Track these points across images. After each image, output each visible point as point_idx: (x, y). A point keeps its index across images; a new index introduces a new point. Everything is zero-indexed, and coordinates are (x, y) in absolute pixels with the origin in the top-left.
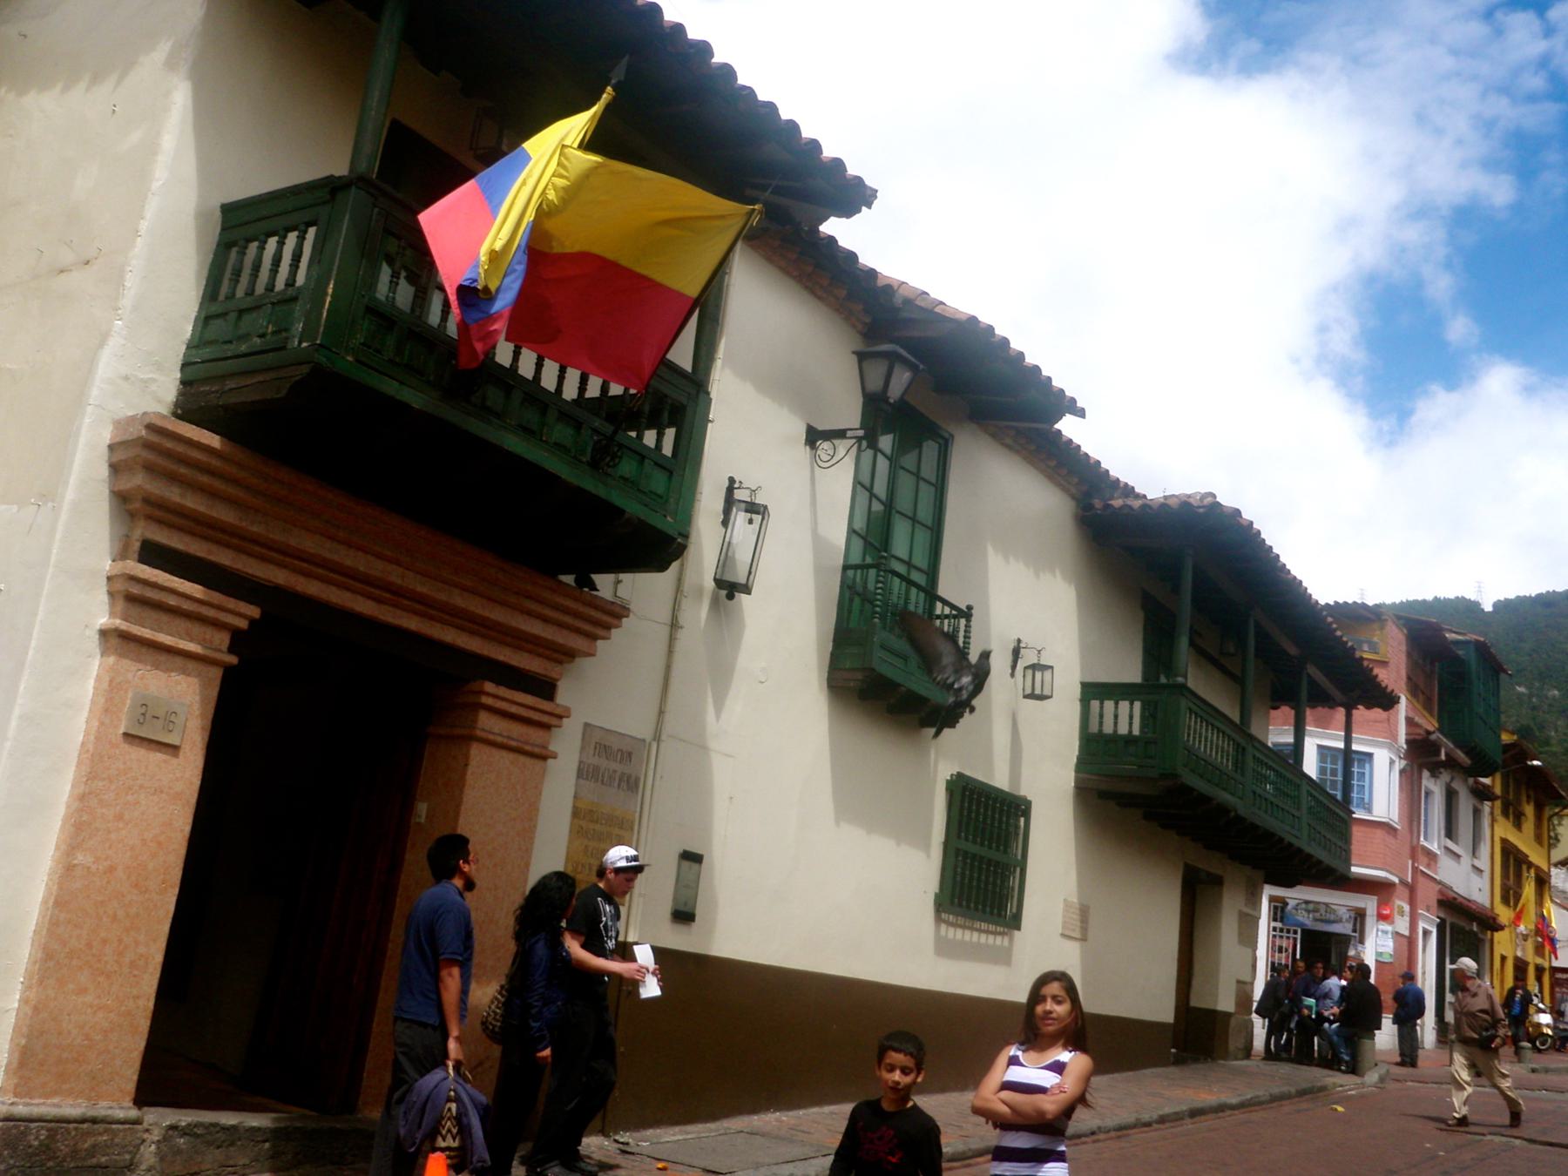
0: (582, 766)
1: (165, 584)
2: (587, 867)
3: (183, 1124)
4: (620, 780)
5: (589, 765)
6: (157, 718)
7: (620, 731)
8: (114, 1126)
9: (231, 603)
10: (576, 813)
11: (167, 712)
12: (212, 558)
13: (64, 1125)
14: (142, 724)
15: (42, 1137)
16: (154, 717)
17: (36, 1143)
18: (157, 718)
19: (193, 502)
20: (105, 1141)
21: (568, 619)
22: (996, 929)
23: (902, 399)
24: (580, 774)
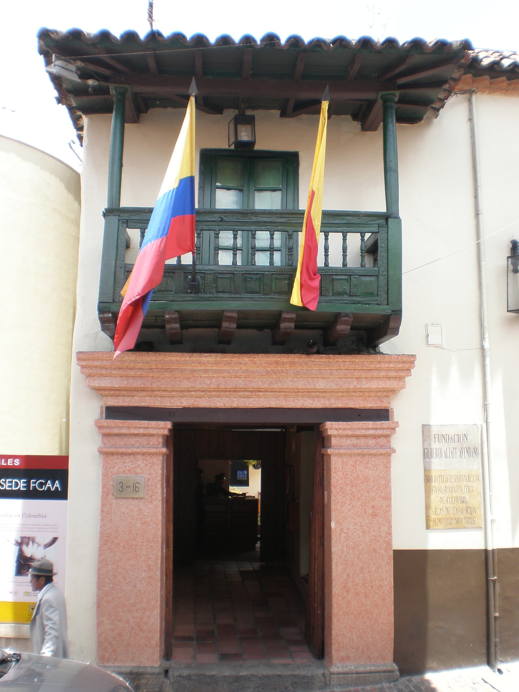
19: (116, 383)
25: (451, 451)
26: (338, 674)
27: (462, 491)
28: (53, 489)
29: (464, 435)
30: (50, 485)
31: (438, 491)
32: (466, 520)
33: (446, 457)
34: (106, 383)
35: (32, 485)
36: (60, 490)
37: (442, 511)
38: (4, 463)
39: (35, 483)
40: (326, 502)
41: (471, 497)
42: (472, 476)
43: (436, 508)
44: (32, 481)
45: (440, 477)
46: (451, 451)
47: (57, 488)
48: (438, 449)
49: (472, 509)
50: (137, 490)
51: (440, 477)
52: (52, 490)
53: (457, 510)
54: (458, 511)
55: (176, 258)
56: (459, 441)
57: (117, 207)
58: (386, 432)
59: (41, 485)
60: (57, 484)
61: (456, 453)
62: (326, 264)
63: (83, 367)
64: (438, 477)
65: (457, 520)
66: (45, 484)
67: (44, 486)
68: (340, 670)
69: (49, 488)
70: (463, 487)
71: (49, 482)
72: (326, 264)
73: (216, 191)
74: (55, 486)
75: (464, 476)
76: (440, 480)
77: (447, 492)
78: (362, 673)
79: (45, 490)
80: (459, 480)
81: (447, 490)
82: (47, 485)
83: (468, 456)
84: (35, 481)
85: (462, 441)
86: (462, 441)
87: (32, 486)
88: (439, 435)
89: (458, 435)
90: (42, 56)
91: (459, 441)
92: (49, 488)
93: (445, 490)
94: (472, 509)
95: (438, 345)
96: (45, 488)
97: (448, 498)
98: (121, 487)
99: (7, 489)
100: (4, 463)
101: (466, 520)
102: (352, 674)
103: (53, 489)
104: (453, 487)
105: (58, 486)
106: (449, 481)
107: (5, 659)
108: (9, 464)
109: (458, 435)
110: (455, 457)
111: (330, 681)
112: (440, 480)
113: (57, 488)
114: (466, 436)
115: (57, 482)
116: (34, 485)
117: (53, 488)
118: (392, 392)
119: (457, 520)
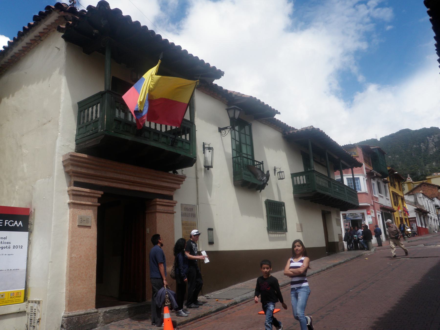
3: (108, 311)
4: (191, 215)
8: (92, 314)
9: (96, 192)
12: (90, 182)
13: (81, 316)
15: (76, 320)
23: (238, 117)
24: (182, 215)
28: (18, 225)
30: (17, 224)
33: (187, 216)
35: (6, 223)
36: (22, 226)
39: (7, 222)
40: (149, 232)
44: (6, 221)
47: (20, 225)
52: (18, 226)
55: (255, 162)
57: (359, 203)
58: (172, 204)
59: (11, 223)
60: (20, 223)
62: (303, 176)
66: (14, 223)
67: (13, 224)
69: (16, 225)
71: (16, 221)
72: (303, 176)
74: (20, 224)
79: (14, 226)
82: (15, 224)
84: (8, 221)
90: (376, 238)
92: (16, 225)
96: (13, 225)
98: (81, 220)
103: (18, 226)
105: (21, 224)
107: (260, 191)
113: (20, 225)
115: (21, 222)
116: (7, 223)
117: (18, 225)
118: (174, 189)
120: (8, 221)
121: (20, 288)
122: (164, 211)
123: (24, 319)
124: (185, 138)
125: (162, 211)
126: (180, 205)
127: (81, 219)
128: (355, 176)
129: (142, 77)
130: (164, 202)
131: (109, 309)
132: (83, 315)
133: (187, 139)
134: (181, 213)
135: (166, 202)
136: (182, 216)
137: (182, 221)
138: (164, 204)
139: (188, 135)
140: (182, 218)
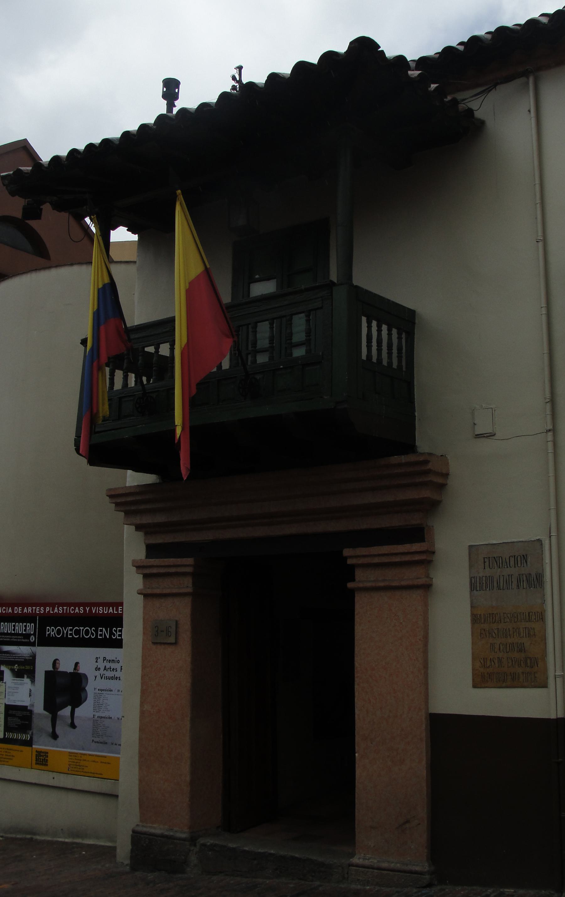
0: (473, 581)
1: (148, 565)
2: (496, 661)
3: (209, 844)
4: (519, 581)
5: (480, 578)
6: (163, 631)
7: (506, 541)
8: (175, 841)
9: (179, 561)
10: (475, 619)
11: (167, 627)
12: (176, 540)
13: (155, 838)
14: (501, 643)
15: (147, 842)
16: (161, 631)
17: (145, 845)
18: (163, 631)
19: (160, 518)
20: (368, 886)
21: (130, 499)
22: (13, 610)
23: (528, 78)
24: (473, 587)
25: (505, 579)
26: (357, 866)
27: (520, 634)
29: (522, 556)
31: (488, 634)
32: (524, 675)
34: (146, 520)
37: (492, 662)
38: (116, 611)
41: (531, 644)
42: (533, 614)
43: (485, 659)
45: (491, 615)
46: (505, 579)
48: (488, 578)
49: (533, 660)
50: (170, 635)
51: (491, 615)
53: (512, 661)
54: (514, 662)
56: (516, 565)
61: (512, 582)
63: (117, 504)
64: (489, 615)
65: (512, 675)
68: (360, 862)
70: (522, 630)
73: (268, 279)
75: (522, 614)
76: (491, 620)
77: (499, 637)
78: (384, 869)
80: (516, 620)
81: (499, 633)
83: (527, 586)
84: (72, 628)
85: (519, 565)
86: (519, 565)
87: (70, 633)
88: (489, 558)
89: (514, 556)
91: (516, 565)
93: (496, 633)
94: (533, 660)
95: (487, 435)
97: (501, 645)
99: (118, 638)
100: (116, 611)
101: (524, 675)
102: (373, 868)
104: (508, 629)
106: (502, 620)
108: (119, 612)
109: (514, 556)
110: (511, 588)
111: (347, 873)
112: (491, 620)
114: (525, 557)
116: (71, 632)
119: (512, 675)
120: (72, 628)
121: (89, 750)
122: (373, 584)
123: (528, 658)
124: (225, 369)
125: (368, 585)
126: (467, 552)
127: (157, 629)
128: (131, 385)
129: (111, 244)
130: (375, 556)
131: (212, 842)
132: (159, 838)
133: (386, 326)
134: (468, 581)
135: (379, 555)
136: (472, 589)
137: (472, 607)
138: (376, 560)
139: (118, 385)
140: (471, 596)
